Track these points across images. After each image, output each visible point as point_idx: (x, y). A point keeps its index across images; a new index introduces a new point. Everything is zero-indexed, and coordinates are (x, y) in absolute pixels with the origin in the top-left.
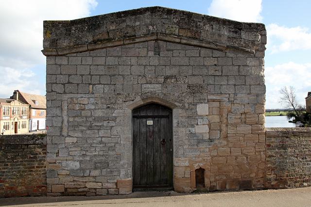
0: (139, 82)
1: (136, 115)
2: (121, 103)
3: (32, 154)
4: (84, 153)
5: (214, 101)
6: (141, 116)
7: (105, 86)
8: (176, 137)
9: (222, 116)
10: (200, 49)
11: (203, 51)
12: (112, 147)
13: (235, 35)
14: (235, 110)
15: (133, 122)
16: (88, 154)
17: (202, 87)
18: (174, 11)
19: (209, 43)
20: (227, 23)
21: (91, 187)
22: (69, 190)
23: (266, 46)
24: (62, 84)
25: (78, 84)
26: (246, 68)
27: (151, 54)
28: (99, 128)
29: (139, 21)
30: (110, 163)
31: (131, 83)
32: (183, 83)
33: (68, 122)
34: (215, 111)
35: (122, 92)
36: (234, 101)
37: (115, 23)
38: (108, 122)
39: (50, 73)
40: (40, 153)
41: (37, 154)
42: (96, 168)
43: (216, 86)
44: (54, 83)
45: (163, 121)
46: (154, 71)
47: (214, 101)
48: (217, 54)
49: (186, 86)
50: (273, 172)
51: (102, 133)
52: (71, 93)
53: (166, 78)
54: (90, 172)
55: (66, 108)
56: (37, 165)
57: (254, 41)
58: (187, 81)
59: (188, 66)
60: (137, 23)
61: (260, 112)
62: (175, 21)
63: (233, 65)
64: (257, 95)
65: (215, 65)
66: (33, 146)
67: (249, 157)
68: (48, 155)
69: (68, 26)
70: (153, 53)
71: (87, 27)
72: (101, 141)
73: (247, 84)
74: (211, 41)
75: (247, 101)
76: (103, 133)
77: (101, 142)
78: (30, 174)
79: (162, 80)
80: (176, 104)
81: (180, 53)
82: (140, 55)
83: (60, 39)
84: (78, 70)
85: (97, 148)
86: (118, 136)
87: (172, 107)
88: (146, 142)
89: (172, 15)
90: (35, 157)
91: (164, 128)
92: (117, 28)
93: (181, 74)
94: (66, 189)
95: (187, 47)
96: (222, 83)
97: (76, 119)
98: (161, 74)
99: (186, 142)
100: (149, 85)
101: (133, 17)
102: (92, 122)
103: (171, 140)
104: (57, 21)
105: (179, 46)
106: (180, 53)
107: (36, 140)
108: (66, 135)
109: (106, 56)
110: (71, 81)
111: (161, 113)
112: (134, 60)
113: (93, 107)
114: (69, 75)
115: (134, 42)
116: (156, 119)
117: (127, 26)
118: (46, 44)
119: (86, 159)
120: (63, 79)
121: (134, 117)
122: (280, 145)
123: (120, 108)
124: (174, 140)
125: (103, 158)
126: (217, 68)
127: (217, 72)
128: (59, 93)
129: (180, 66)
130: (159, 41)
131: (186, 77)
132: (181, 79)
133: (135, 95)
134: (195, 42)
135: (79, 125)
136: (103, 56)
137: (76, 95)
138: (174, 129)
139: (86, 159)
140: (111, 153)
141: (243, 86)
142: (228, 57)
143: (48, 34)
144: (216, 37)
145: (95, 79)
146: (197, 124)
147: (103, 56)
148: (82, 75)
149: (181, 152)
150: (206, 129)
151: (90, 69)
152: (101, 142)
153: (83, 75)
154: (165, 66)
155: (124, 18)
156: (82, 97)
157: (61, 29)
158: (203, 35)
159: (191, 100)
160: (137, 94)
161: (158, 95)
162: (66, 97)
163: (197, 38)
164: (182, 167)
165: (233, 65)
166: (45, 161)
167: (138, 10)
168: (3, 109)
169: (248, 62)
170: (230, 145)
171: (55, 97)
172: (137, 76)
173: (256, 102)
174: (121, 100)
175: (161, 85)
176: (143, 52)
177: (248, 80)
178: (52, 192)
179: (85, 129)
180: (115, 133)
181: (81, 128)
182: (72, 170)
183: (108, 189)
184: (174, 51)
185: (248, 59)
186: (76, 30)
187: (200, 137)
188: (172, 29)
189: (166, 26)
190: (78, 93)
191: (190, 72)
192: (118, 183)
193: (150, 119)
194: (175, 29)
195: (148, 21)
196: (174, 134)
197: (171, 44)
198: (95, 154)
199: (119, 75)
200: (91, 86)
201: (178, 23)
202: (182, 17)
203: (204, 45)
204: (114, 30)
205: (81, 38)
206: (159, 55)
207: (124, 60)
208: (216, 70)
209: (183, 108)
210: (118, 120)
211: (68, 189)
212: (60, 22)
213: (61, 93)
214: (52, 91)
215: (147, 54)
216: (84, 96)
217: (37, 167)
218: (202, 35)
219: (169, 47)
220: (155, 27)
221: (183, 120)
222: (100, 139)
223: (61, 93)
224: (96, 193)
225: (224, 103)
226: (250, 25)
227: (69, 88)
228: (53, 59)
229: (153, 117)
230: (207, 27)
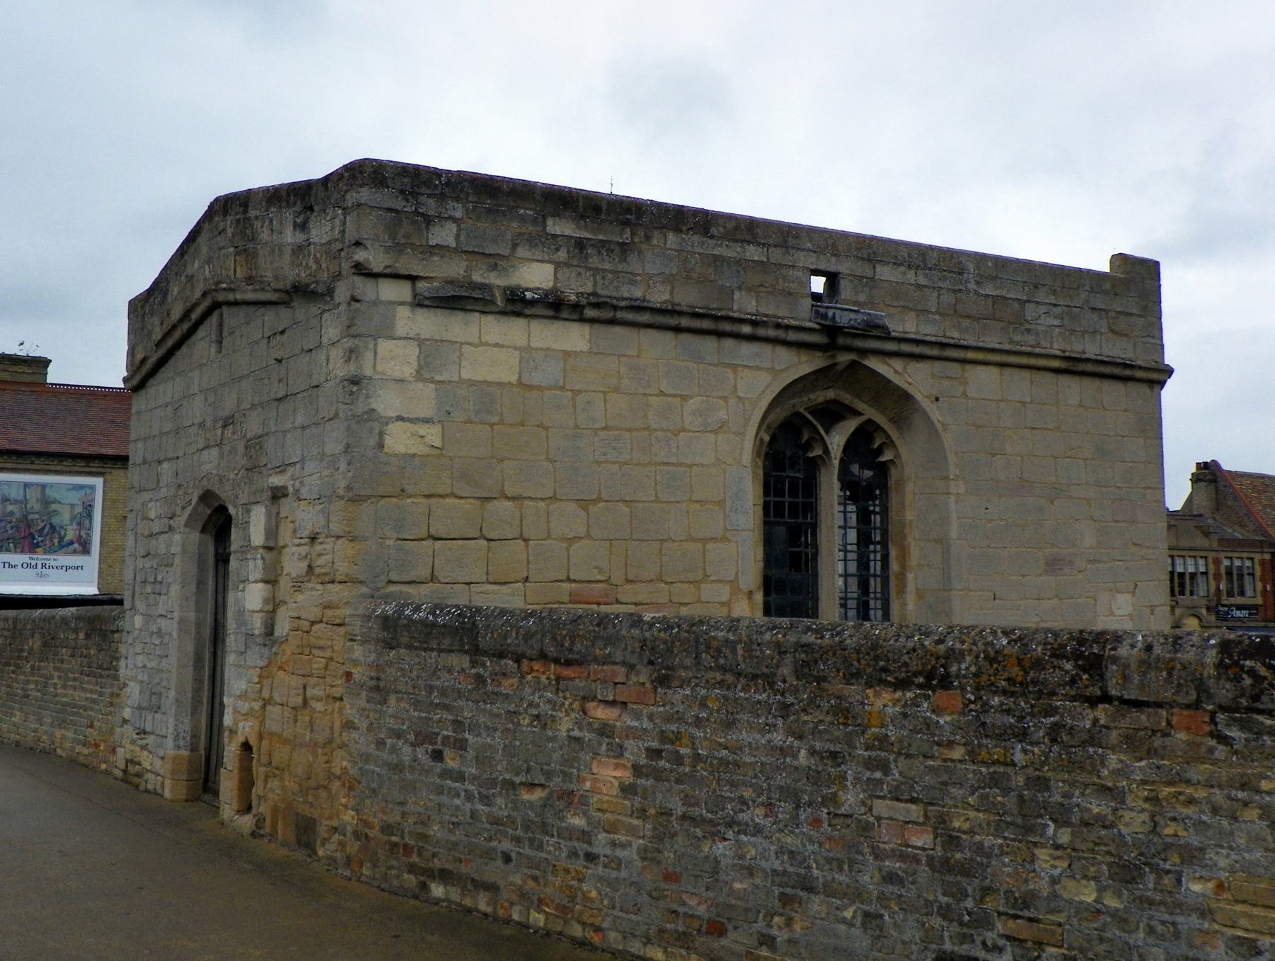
13: (399, 204)
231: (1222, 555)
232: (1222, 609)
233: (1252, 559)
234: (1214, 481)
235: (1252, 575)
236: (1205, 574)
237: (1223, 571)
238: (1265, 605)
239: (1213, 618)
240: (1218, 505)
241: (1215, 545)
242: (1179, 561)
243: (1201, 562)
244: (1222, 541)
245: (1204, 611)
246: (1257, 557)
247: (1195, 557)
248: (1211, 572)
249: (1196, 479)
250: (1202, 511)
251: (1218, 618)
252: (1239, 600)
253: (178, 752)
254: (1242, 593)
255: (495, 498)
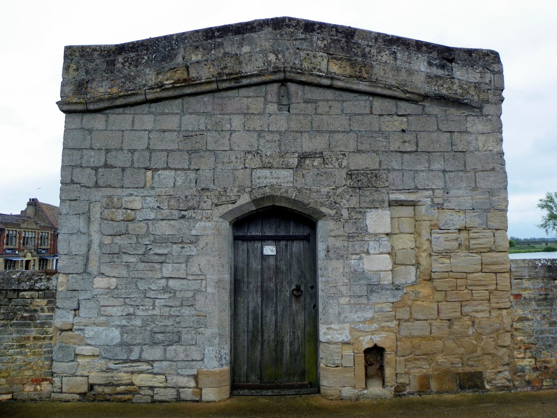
0: (247, 166)
1: (241, 234)
2: (209, 207)
3: (26, 311)
4: (131, 310)
5: (402, 204)
6: (252, 236)
7: (178, 172)
8: (324, 279)
9: (419, 235)
10: (371, 98)
11: (378, 103)
12: (188, 299)
13: (440, 72)
14: (446, 223)
15: (235, 247)
16: (139, 313)
17: (376, 176)
18: (317, 26)
19: (390, 88)
20: (424, 48)
21: (143, 383)
22: (99, 389)
23: (504, 94)
24: (92, 168)
25: (123, 169)
26: (466, 136)
27: (272, 108)
28: (163, 259)
29: (250, 44)
30: (183, 333)
31: (231, 166)
32: (337, 166)
33: (101, 245)
34: (407, 225)
35: (212, 186)
36: (443, 204)
37: (201, 50)
38: (183, 248)
39: (71, 145)
40: (42, 310)
41: (36, 311)
42: (154, 344)
43: (405, 175)
44: (76, 166)
45: (297, 247)
46: (277, 143)
47: (402, 205)
48: (404, 107)
49: (344, 173)
50: (528, 354)
51: (168, 269)
52: (110, 186)
53: (303, 157)
54: (142, 351)
55: (98, 216)
56: (34, 334)
57: (479, 83)
58: (344, 164)
59: (348, 132)
60: (246, 49)
61: (497, 226)
62: (321, 44)
63: (439, 129)
64: (491, 192)
65: (403, 131)
66: (30, 293)
67: (477, 321)
68: (58, 312)
69: (110, 56)
70: (275, 106)
71: (146, 57)
72: (167, 286)
73: (468, 168)
74: (394, 83)
75: (468, 205)
76: (170, 269)
77: (165, 289)
78: (20, 353)
79: (294, 161)
80: (324, 210)
81: (330, 107)
82: (251, 111)
83: (94, 80)
84: (126, 140)
85: (157, 301)
86: (201, 277)
87: (316, 217)
88: (262, 291)
89: (315, 34)
90: (32, 318)
91: (299, 262)
92: (205, 58)
93: (335, 150)
94: (91, 387)
95: (346, 95)
96: (418, 168)
97: (118, 240)
98: (293, 150)
99: (344, 289)
100: (267, 172)
101: (237, 38)
102: (150, 247)
103: (314, 287)
104: (89, 47)
105: (329, 94)
106: (330, 107)
107: (36, 282)
108: (95, 273)
109: (183, 113)
110: (111, 162)
111: (293, 231)
112: (237, 122)
113: (152, 216)
114: (108, 151)
115: (238, 84)
116: (283, 243)
117: (226, 54)
118: (68, 89)
119: (133, 322)
120: (97, 159)
121: (236, 238)
122: (541, 295)
123: (207, 218)
124: (320, 286)
125: (170, 322)
126: (407, 137)
127: (407, 144)
128: (85, 186)
129: (331, 132)
130: (289, 84)
131: (344, 155)
132: (334, 159)
133: (238, 191)
134: (362, 86)
135: (120, 253)
136: (177, 114)
137: (119, 190)
138: (321, 263)
139: (133, 322)
140: (186, 311)
141: (461, 174)
142: (429, 115)
143: (71, 70)
144: (404, 74)
145: (159, 160)
146: (368, 253)
147: (177, 114)
148: (133, 151)
149: (333, 310)
150: (385, 262)
151: (149, 138)
152: (165, 289)
153: (135, 150)
154: (301, 132)
155: (219, 40)
156: (131, 195)
157: (98, 61)
158: (378, 71)
159: (354, 202)
160: (242, 189)
161: (286, 192)
162: (97, 195)
163: (365, 78)
164: (335, 343)
165: (439, 129)
166: (50, 325)
167: (247, 24)
168: (7, 232)
169: (468, 125)
170: (439, 296)
171: (77, 194)
172: (242, 154)
173: (488, 206)
174: (209, 202)
175: (291, 171)
176: (256, 105)
177: (471, 162)
178: (61, 392)
179: (133, 260)
180: (195, 269)
181: (126, 258)
182: (107, 347)
183: (178, 388)
184: (320, 103)
185: (468, 118)
186: (125, 62)
187: (374, 281)
188: (313, 60)
189: (303, 54)
190: (122, 187)
191: (352, 146)
192: (200, 377)
193: (269, 242)
194: (320, 59)
195: (267, 45)
196: (320, 272)
197: (313, 89)
198: (154, 312)
199: (207, 150)
200: (149, 173)
201: (326, 49)
202: (336, 38)
203: (379, 91)
204: (198, 62)
205: (134, 78)
206: (289, 111)
207: (218, 120)
208: (405, 142)
209: (338, 218)
210: (202, 243)
211: (96, 387)
212: (94, 49)
213: (88, 187)
214: (72, 182)
215: (265, 109)
216: (135, 193)
217: (35, 338)
218: (375, 71)
219: (309, 96)
220: (280, 56)
221: (339, 243)
222: (163, 282)
223: (88, 187)
224: (152, 397)
225: (423, 209)
226: (470, 52)
227: (107, 176)
228: (77, 118)
229: (276, 239)
230: (385, 57)
231: (40, 231)
232: (39, 250)
233: (16, 231)
234: (35, 205)
235: (48, 238)
236: (34, 238)
237: (40, 237)
238: (50, 249)
239: (35, 253)
240: (36, 213)
241: (38, 228)
242: (27, 233)
243: (34, 233)
244: (41, 226)
245: (33, 251)
246: (50, 232)
247: (32, 232)
248: (37, 237)
249: (29, 204)
250: (30, 216)
251: (37, 253)
252: (43, 247)
253: (221, 369)
254: (44, 245)
255: (397, 234)
